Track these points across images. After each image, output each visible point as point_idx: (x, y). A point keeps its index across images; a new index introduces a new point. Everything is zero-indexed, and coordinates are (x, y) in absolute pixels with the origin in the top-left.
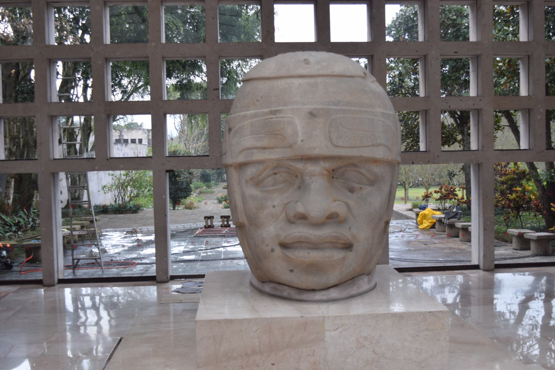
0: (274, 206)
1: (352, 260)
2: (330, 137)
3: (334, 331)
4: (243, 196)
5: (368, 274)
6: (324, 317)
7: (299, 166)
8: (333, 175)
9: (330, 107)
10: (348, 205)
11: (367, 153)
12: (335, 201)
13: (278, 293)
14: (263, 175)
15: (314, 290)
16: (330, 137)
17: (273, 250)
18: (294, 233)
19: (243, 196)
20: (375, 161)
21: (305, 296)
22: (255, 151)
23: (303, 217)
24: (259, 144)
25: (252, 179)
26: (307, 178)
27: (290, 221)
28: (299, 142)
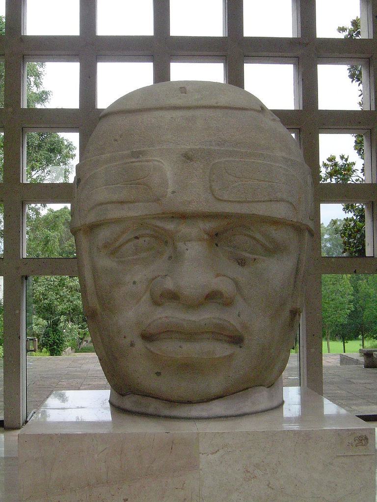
0: (134, 283)
1: (242, 359)
2: (211, 187)
3: (212, 454)
4: (94, 269)
5: (270, 386)
6: (198, 434)
7: (170, 226)
8: (215, 239)
9: (212, 148)
10: (236, 284)
11: (261, 210)
12: (218, 275)
13: (143, 410)
14: (121, 240)
15: (190, 402)
16: (211, 187)
17: (132, 345)
18: (160, 318)
19: (94, 269)
20: (276, 222)
21: (177, 412)
22: (109, 206)
23: (173, 297)
24: (115, 197)
25: (106, 246)
26: (180, 245)
27: (156, 302)
28: (169, 195)
